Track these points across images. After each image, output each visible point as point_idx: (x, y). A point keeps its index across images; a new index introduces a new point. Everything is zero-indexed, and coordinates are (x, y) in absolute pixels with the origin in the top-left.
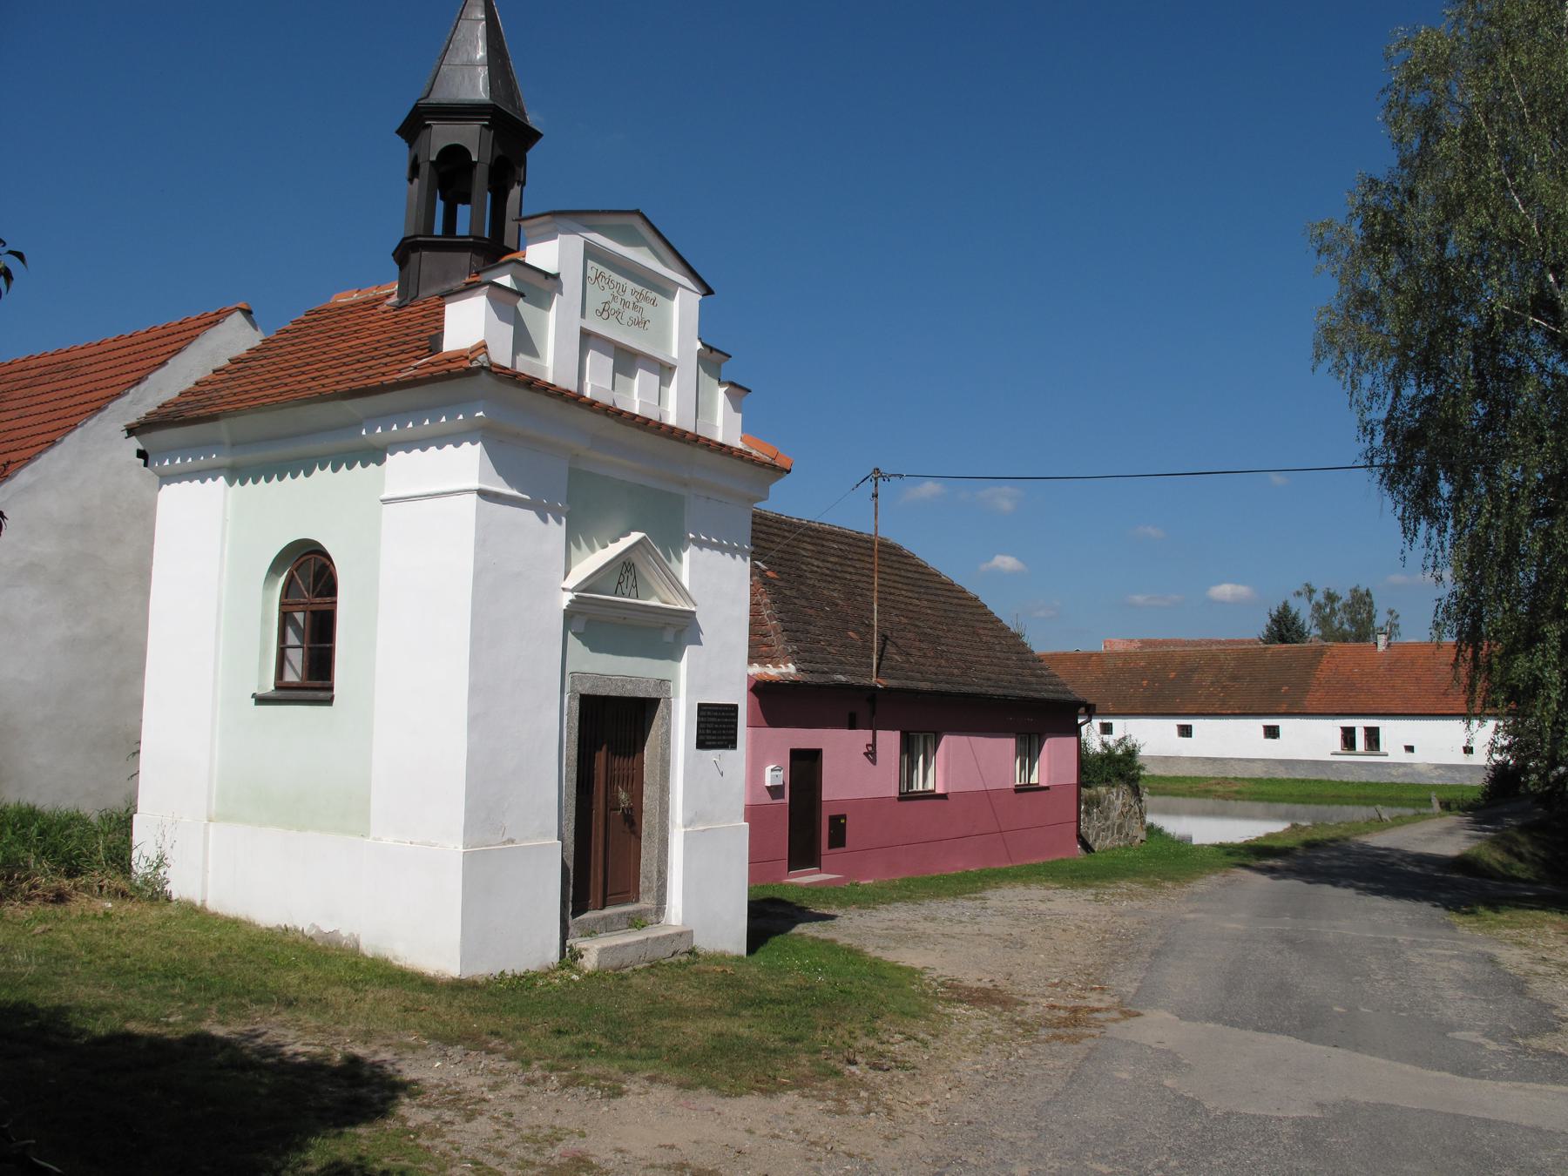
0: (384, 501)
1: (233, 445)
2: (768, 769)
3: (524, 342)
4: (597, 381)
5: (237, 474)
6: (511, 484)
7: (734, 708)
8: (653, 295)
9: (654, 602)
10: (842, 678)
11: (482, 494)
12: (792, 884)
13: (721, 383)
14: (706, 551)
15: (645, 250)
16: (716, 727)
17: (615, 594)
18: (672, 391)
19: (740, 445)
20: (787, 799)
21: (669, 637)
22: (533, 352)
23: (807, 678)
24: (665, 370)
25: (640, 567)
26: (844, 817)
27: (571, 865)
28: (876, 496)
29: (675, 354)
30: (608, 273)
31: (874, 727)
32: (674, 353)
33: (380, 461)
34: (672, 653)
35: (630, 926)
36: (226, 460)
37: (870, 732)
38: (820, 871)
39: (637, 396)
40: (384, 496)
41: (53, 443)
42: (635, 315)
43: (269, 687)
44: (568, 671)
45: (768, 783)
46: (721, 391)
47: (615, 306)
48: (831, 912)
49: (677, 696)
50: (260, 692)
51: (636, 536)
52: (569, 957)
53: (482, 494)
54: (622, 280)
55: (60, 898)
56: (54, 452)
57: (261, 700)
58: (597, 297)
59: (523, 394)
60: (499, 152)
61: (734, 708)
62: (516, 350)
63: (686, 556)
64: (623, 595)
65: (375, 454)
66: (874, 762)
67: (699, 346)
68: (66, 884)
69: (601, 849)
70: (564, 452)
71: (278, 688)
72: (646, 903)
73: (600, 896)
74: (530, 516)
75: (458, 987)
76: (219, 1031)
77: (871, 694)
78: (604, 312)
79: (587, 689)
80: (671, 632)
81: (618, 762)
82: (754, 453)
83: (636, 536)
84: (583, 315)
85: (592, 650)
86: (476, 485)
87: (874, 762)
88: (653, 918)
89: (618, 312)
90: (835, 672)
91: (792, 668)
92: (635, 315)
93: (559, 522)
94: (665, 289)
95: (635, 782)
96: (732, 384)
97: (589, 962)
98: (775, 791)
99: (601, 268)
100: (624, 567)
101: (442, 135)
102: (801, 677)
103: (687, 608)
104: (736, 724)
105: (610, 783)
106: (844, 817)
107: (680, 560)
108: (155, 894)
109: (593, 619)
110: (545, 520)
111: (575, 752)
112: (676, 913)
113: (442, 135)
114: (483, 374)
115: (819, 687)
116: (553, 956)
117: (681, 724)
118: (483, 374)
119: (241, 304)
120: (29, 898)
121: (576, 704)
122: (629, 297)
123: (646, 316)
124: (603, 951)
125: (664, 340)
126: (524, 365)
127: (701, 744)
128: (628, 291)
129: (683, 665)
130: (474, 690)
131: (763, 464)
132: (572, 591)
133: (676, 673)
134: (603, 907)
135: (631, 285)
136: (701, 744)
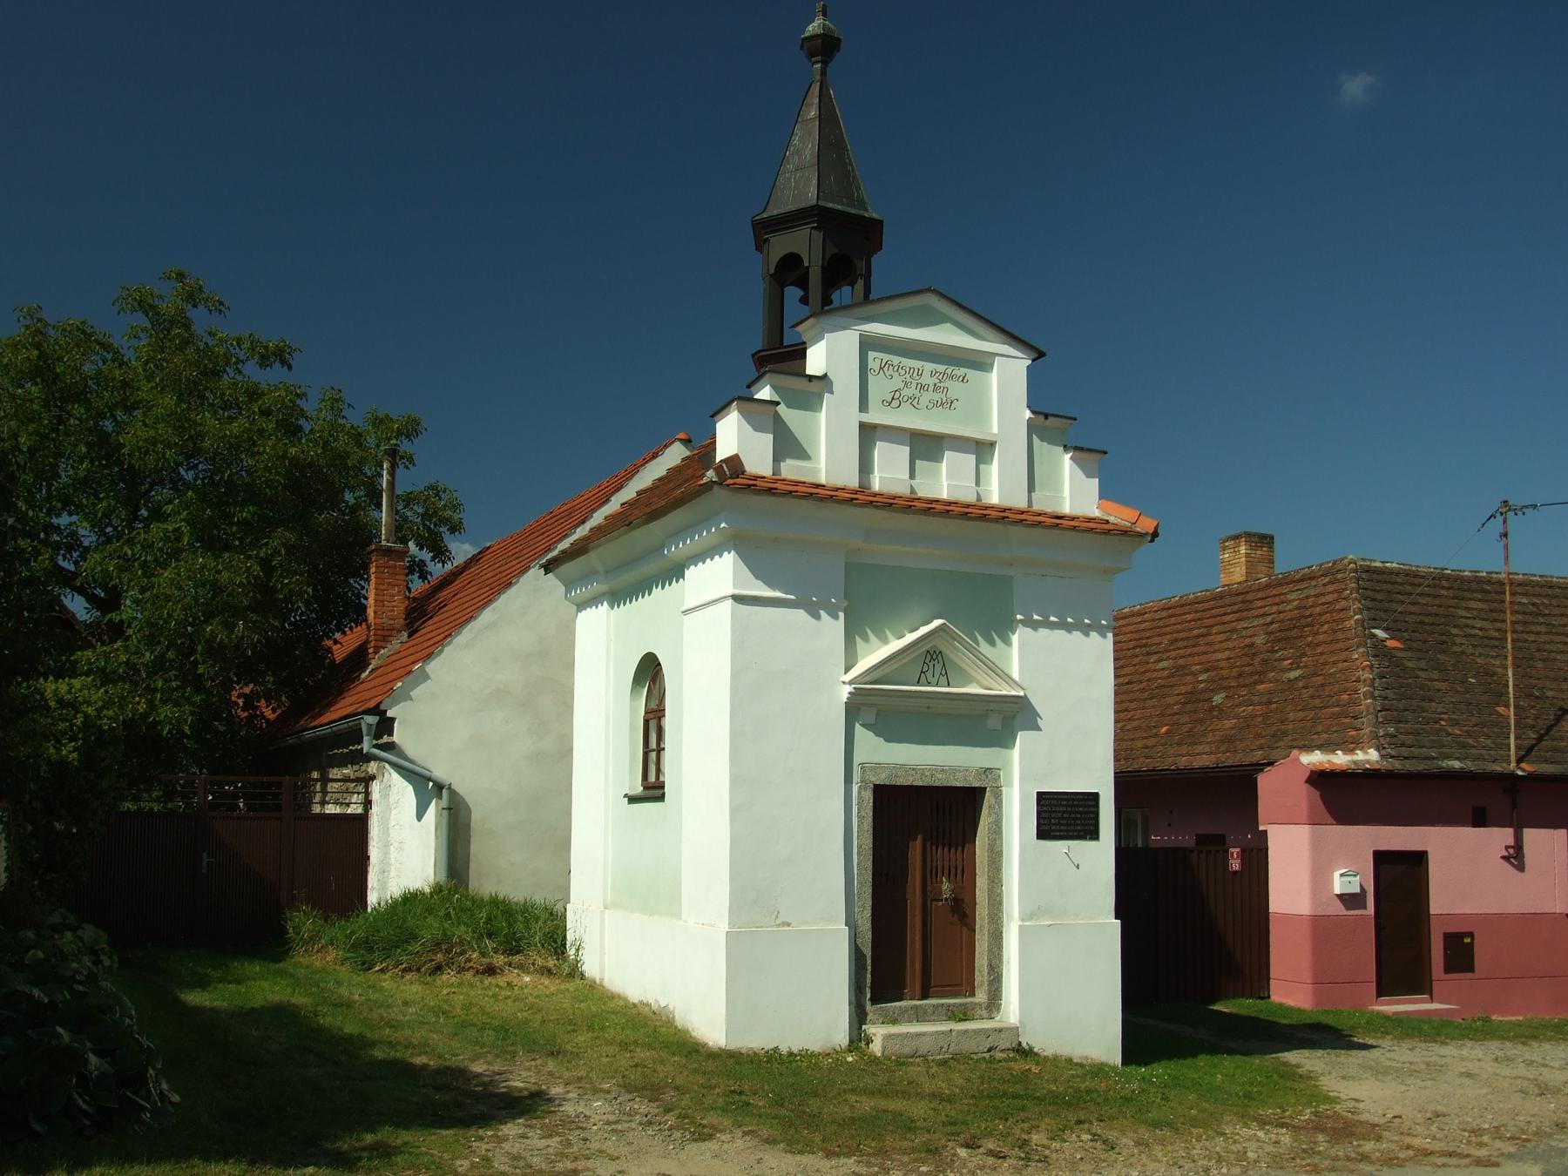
0: (685, 612)
1: (607, 572)
2: (1337, 875)
3: (787, 445)
4: (890, 471)
5: (617, 597)
6: (772, 586)
7: (1094, 797)
8: (963, 371)
9: (973, 689)
10: (1456, 764)
11: (737, 599)
12: (1378, 1013)
13: (1066, 448)
14: (1043, 632)
15: (948, 326)
16: (1063, 816)
17: (918, 683)
18: (994, 470)
19: (1096, 513)
20: (1371, 909)
21: (994, 723)
22: (803, 454)
23: (1397, 765)
24: (982, 449)
25: (947, 652)
26: (1471, 935)
27: (868, 951)
28: (1506, 535)
29: (995, 430)
30: (896, 360)
31: (1518, 825)
32: (995, 428)
33: (679, 575)
34: (1003, 739)
35: (950, 1019)
36: (604, 587)
37: (1510, 831)
38: (1432, 1000)
39: (947, 480)
40: (688, 605)
41: (509, 585)
42: (937, 397)
43: (638, 789)
44: (857, 760)
45: (1337, 891)
46: (1068, 456)
47: (907, 392)
48: (1370, 1042)
49: (1010, 784)
50: (631, 793)
51: (937, 623)
52: (858, 1038)
53: (737, 599)
54: (917, 364)
55: (491, 971)
56: (512, 592)
57: (633, 800)
58: (880, 387)
59: (768, 500)
60: (832, 250)
61: (1094, 797)
62: (777, 458)
63: (1015, 638)
64: (929, 684)
65: (675, 572)
66: (1521, 867)
67: (1028, 414)
68: (499, 960)
69: (918, 939)
70: (836, 549)
71: (645, 788)
72: (981, 997)
73: (918, 986)
74: (800, 614)
75: (730, 1061)
76: (478, 1068)
77: (1509, 782)
78: (894, 400)
79: (882, 779)
80: (1006, 718)
81: (941, 855)
82: (1112, 519)
83: (937, 623)
84: (863, 405)
85: (887, 740)
86: (731, 591)
87: (1521, 867)
88: (984, 1013)
89: (912, 398)
90: (1448, 757)
91: (1373, 755)
92: (937, 397)
93: (836, 617)
94: (980, 363)
95: (964, 874)
96: (1076, 449)
97: (876, 1048)
98: (1349, 900)
99: (886, 357)
100: (929, 657)
101: (782, 245)
102: (1386, 765)
103: (1013, 693)
104: (1097, 814)
105: (930, 874)
106: (1471, 935)
107: (1008, 643)
108: (575, 972)
109: (871, 708)
110: (817, 617)
111: (868, 842)
112: (1012, 1009)
113: (782, 245)
114: (716, 488)
115: (1410, 776)
116: (841, 1037)
117: (1015, 815)
118: (716, 488)
119: (681, 436)
120: (463, 969)
121: (868, 795)
122: (926, 379)
123: (952, 395)
124: (888, 1037)
125: (981, 413)
126: (791, 469)
127: (1043, 834)
128: (926, 374)
129: (1016, 752)
130: (736, 782)
131: (1125, 533)
132: (850, 683)
133: (1009, 762)
134: (924, 996)
135: (929, 367)
136: (1043, 834)
